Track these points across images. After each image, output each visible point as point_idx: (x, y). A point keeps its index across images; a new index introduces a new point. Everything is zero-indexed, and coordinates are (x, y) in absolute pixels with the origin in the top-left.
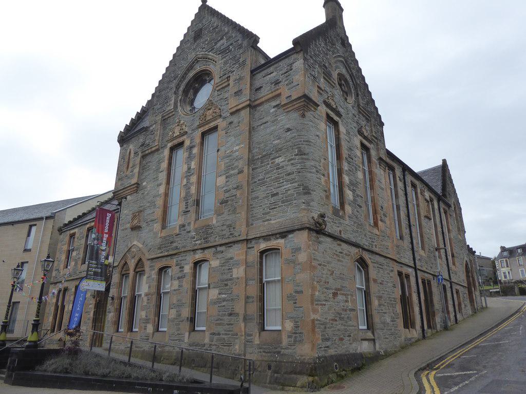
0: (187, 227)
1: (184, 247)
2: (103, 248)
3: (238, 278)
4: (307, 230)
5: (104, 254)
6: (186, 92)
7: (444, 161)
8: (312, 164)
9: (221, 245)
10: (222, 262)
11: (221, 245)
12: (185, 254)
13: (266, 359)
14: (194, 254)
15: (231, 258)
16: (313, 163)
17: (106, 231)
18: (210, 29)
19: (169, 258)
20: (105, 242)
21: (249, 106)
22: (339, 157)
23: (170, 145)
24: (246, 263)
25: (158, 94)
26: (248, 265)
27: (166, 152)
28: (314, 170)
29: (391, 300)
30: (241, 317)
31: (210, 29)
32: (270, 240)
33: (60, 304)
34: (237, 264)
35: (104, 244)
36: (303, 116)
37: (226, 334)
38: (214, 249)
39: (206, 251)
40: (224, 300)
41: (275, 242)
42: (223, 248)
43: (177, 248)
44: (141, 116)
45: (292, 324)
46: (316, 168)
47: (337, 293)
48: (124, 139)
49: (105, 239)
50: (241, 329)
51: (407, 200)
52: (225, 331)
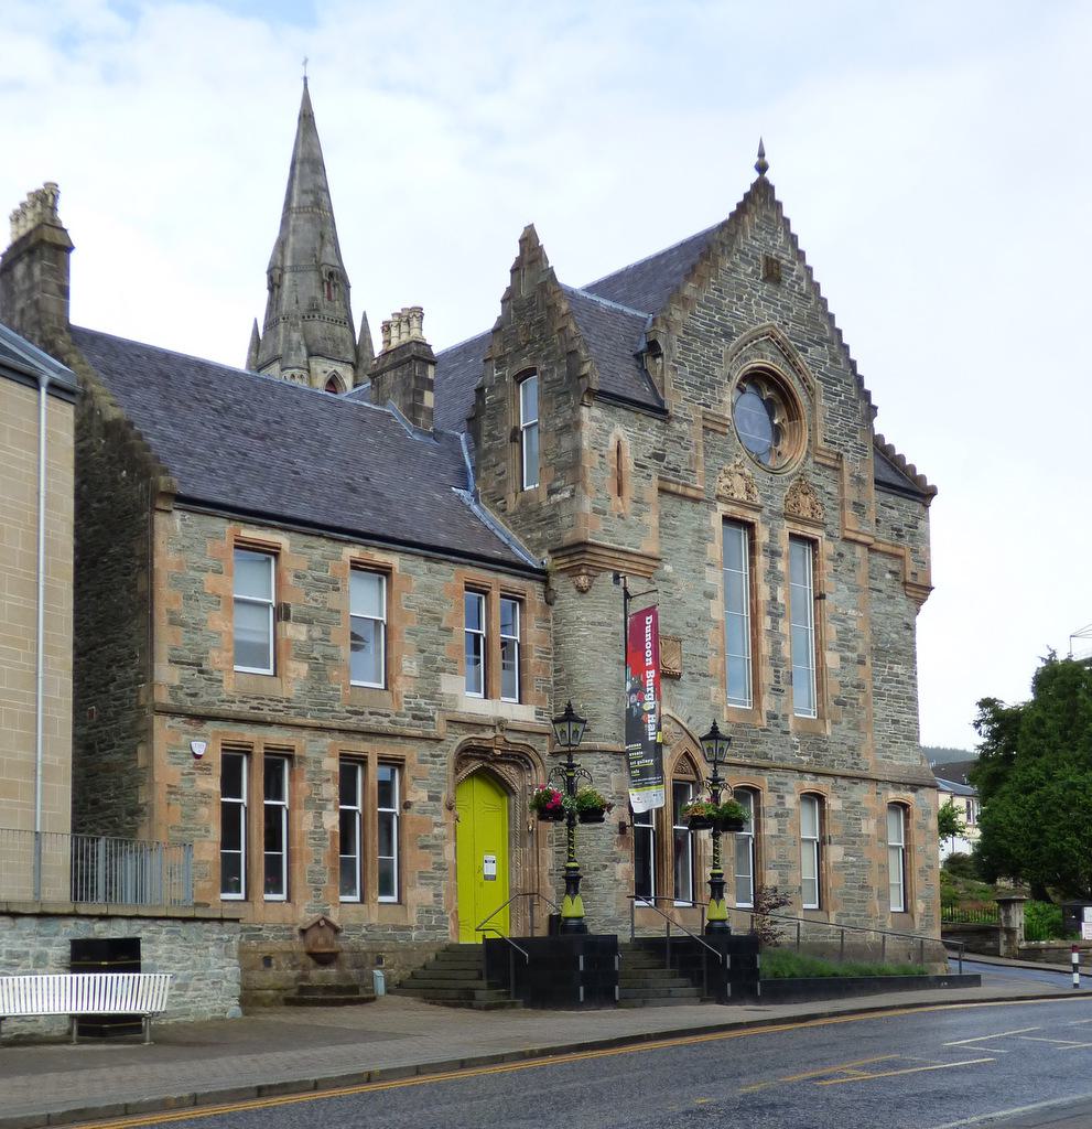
0: (780, 721)
1: (782, 759)
2: (648, 706)
3: (869, 836)
5: (652, 719)
9: (844, 777)
10: (846, 805)
11: (844, 777)
12: (783, 774)
13: (903, 947)
14: (802, 778)
15: (859, 803)
17: (649, 662)
19: (754, 771)
20: (652, 689)
25: (527, 258)
32: (899, 789)
34: (866, 814)
35: (649, 697)
37: (858, 916)
38: (832, 780)
39: (821, 780)
40: (853, 866)
41: (905, 795)
42: (844, 783)
43: (765, 756)
45: (924, 906)
47: (650, 900)
49: (650, 683)
50: (875, 907)
51: (281, 724)
52: (857, 911)
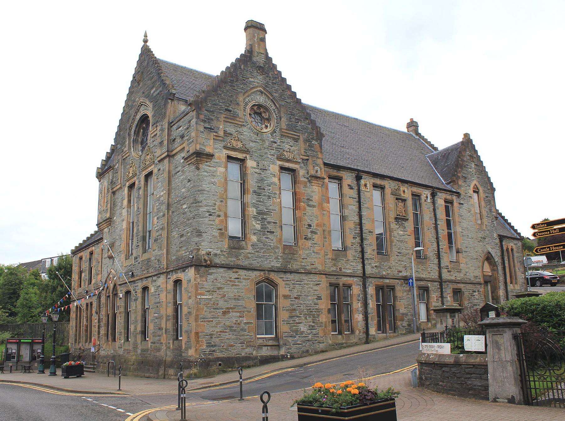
4: (193, 269)
6: (137, 133)
7: (467, 136)
8: (205, 210)
11: (154, 276)
16: (205, 209)
18: (150, 72)
21: (168, 156)
22: (244, 191)
23: (127, 184)
24: (166, 291)
26: (168, 292)
27: (126, 189)
28: (207, 214)
29: (312, 312)
30: (164, 331)
31: (150, 72)
33: (110, 313)
36: (198, 169)
44: (109, 156)
46: (208, 212)
48: (101, 175)
